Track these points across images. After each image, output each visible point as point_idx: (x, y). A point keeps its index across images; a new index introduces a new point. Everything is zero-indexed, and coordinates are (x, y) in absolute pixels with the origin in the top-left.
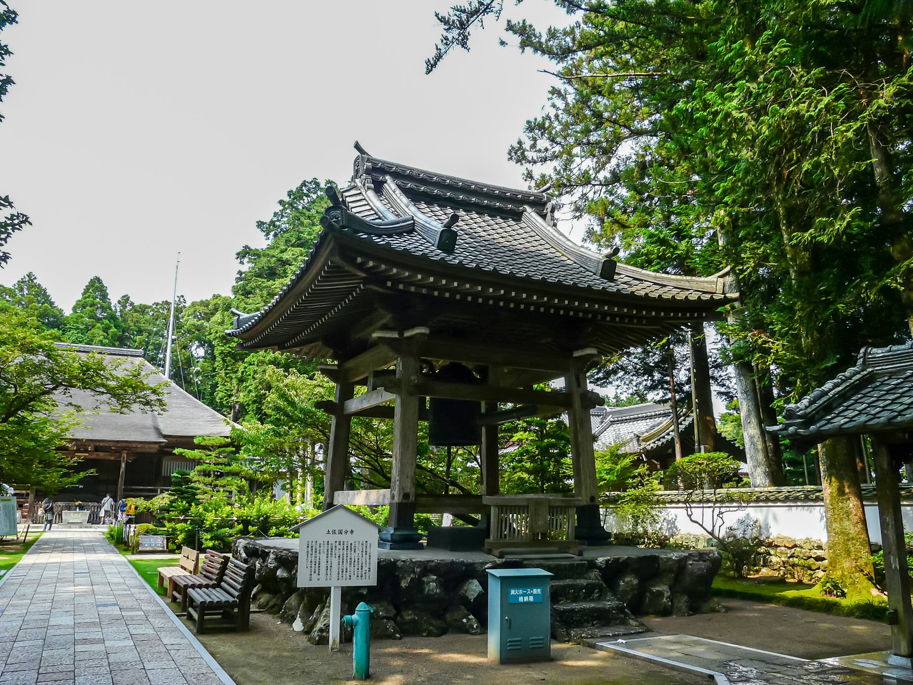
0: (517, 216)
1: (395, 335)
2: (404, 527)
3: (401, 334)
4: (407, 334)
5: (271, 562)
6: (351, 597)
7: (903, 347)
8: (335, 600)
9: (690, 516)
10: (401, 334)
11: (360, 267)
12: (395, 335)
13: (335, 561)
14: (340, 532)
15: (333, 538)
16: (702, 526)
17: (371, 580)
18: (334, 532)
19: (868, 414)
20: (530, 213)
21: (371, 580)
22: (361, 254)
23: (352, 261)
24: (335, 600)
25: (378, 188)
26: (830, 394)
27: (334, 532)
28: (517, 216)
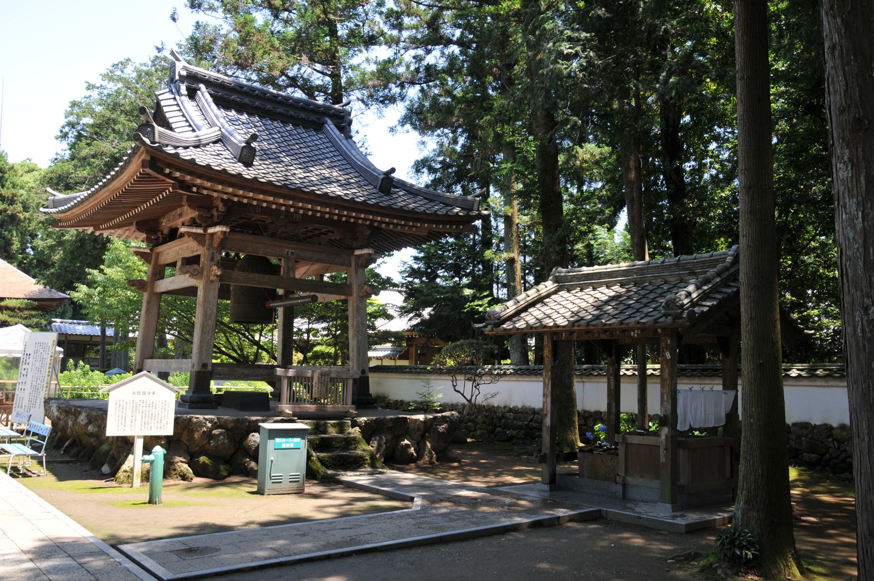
0: (318, 127)
1: (200, 231)
2: (198, 398)
3: (205, 230)
4: (211, 230)
5: (82, 419)
6: (150, 443)
7: (690, 257)
8: (139, 445)
9: (454, 386)
10: (205, 230)
11: (169, 176)
12: (200, 231)
13: (139, 416)
14: (144, 393)
15: (137, 398)
16: (463, 395)
17: (169, 431)
18: (139, 393)
19: (625, 305)
20: (330, 126)
21: (169, 431)
22: (169, 166)
23: (160, 171)
24: (139, 445)
25: (192, 94)
26: (232, 138)
27: (139, 393)
28: (318, 127)
